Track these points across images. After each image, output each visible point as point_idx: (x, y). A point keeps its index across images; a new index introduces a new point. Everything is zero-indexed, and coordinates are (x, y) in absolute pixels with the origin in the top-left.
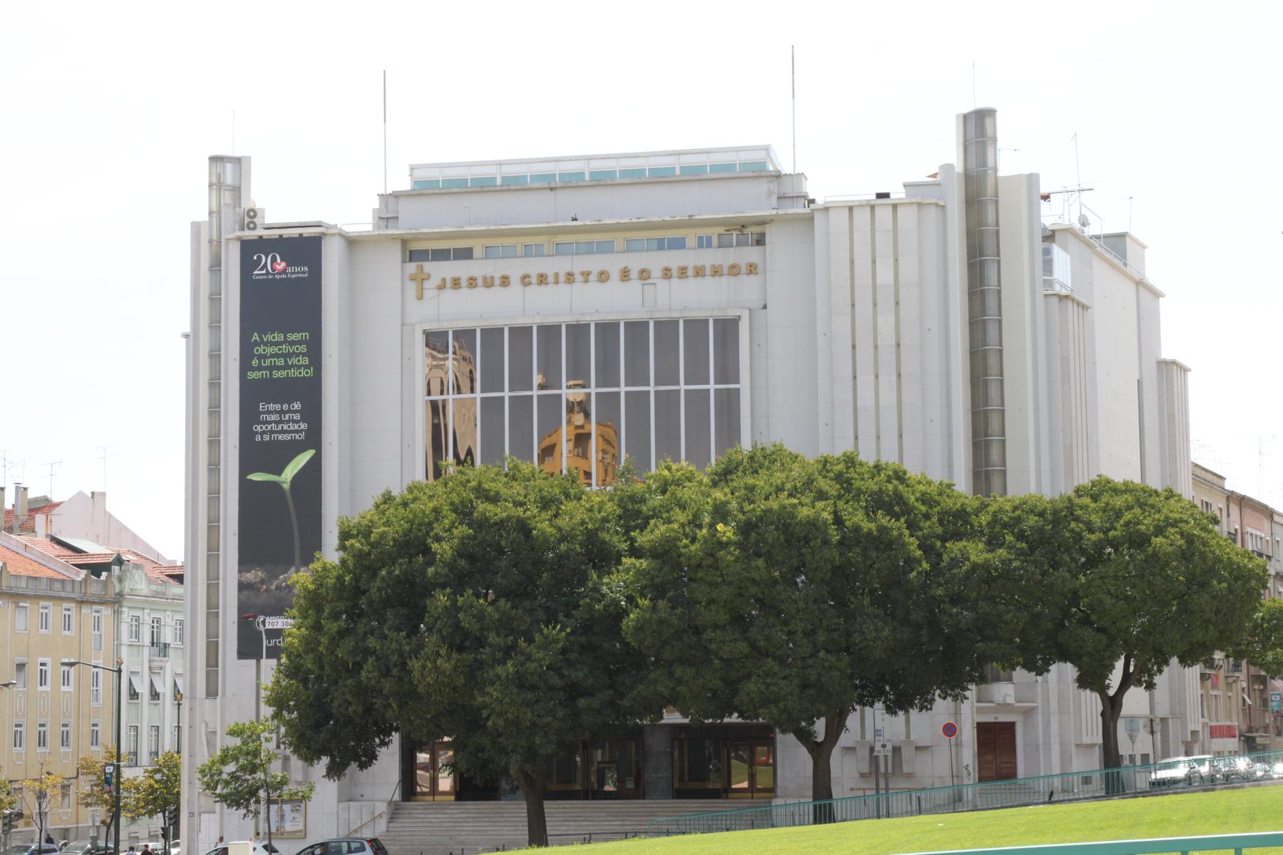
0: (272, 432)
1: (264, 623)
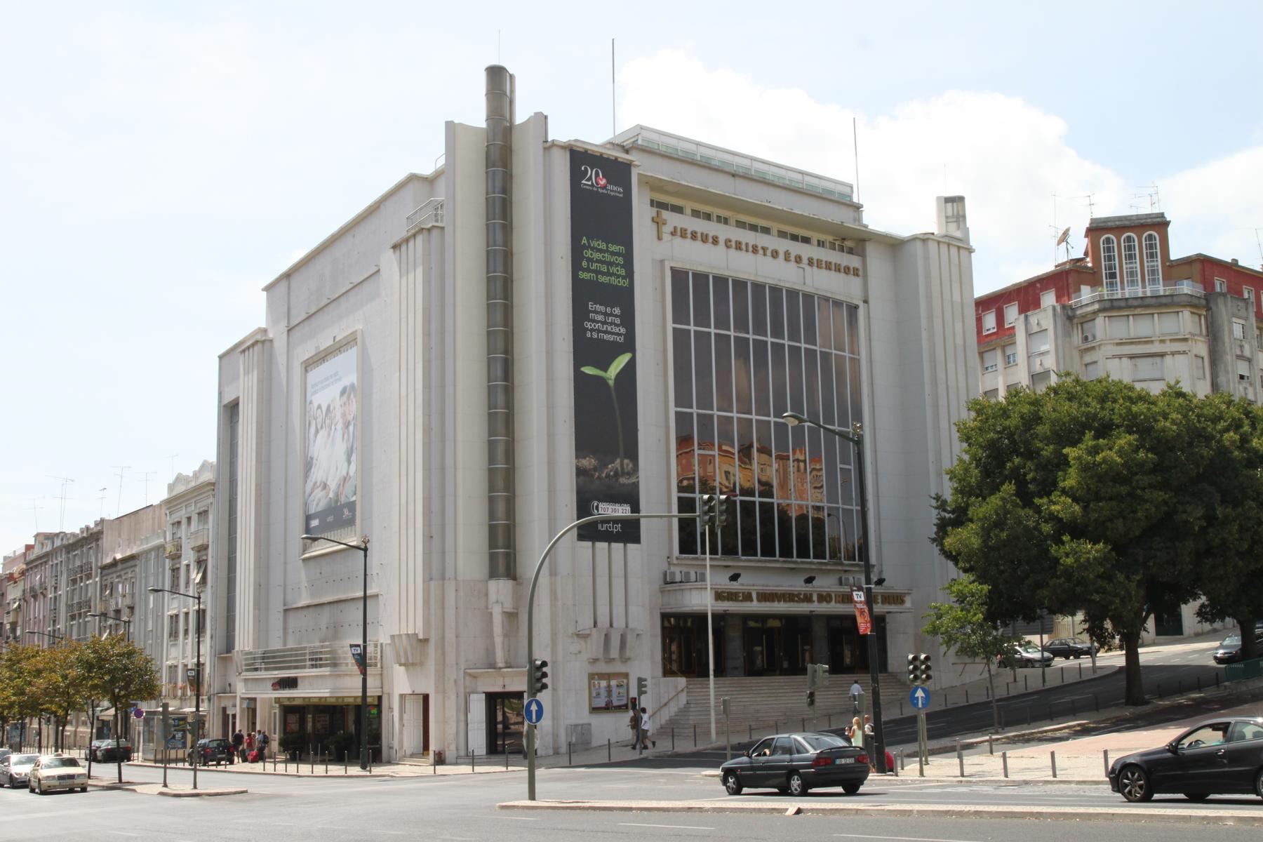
0: (599, 331)
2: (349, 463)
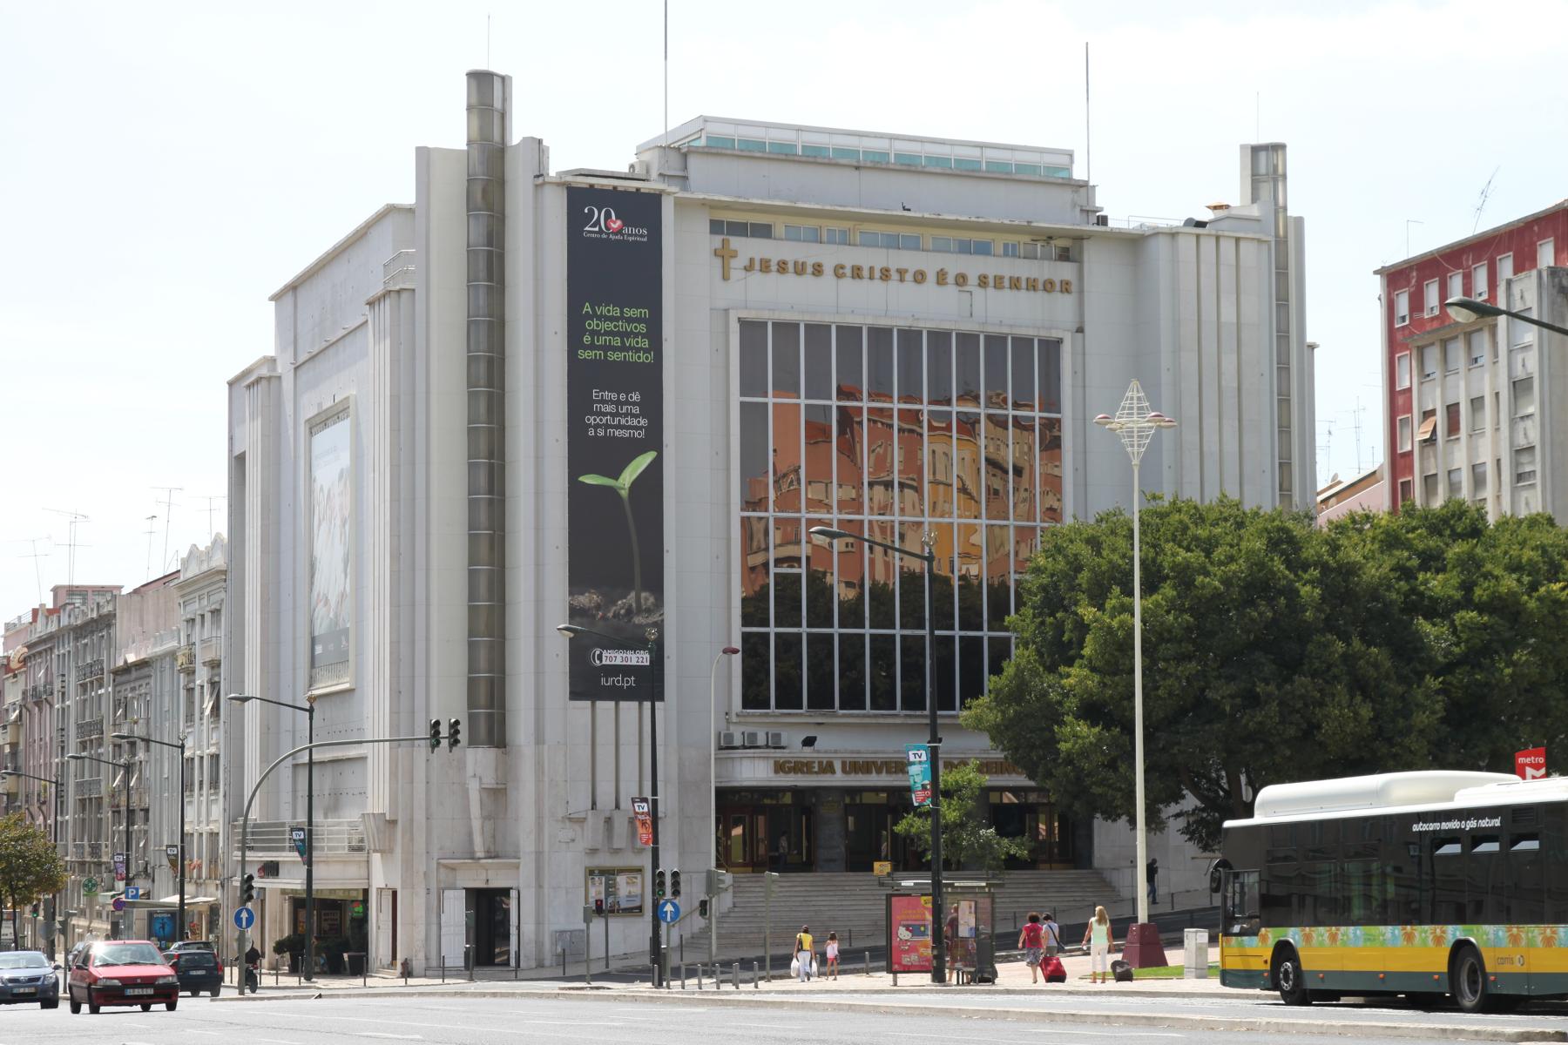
0: (607, 426)
1: (600, 657)
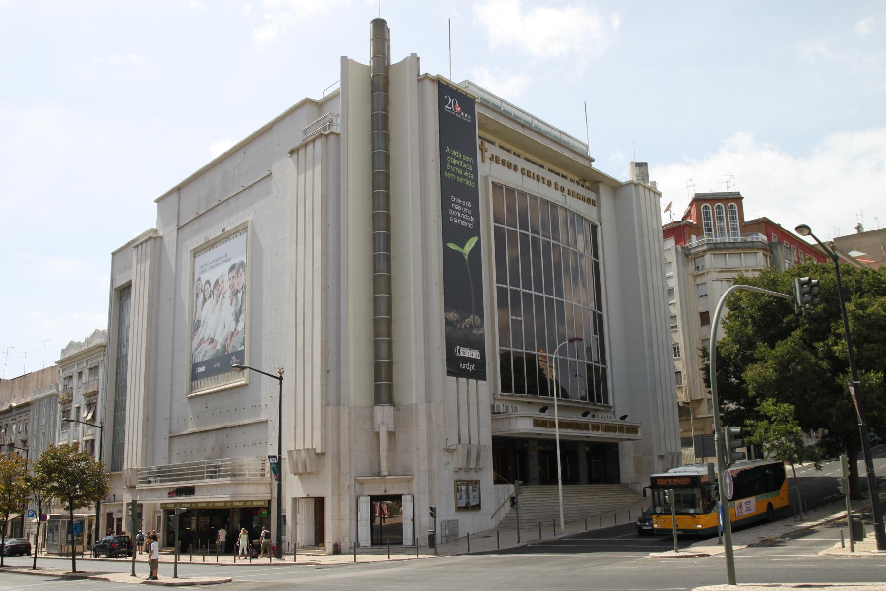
0: (458, 218)
2: (237, 321)
